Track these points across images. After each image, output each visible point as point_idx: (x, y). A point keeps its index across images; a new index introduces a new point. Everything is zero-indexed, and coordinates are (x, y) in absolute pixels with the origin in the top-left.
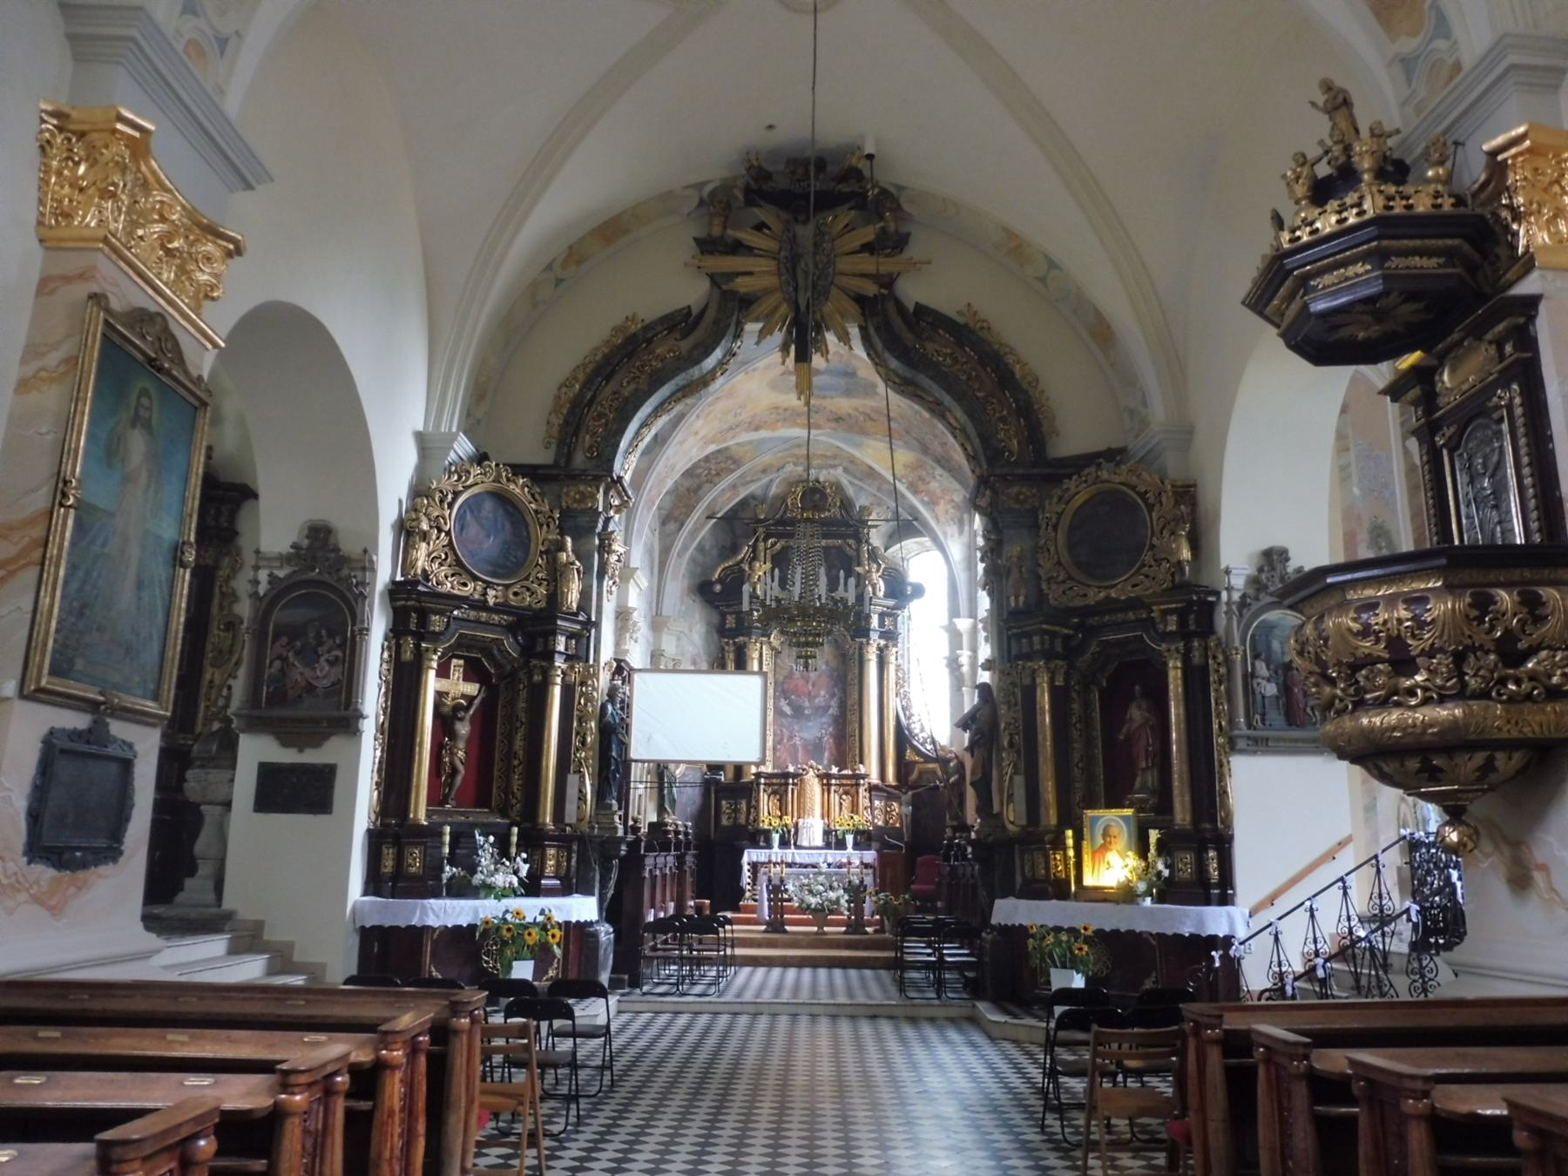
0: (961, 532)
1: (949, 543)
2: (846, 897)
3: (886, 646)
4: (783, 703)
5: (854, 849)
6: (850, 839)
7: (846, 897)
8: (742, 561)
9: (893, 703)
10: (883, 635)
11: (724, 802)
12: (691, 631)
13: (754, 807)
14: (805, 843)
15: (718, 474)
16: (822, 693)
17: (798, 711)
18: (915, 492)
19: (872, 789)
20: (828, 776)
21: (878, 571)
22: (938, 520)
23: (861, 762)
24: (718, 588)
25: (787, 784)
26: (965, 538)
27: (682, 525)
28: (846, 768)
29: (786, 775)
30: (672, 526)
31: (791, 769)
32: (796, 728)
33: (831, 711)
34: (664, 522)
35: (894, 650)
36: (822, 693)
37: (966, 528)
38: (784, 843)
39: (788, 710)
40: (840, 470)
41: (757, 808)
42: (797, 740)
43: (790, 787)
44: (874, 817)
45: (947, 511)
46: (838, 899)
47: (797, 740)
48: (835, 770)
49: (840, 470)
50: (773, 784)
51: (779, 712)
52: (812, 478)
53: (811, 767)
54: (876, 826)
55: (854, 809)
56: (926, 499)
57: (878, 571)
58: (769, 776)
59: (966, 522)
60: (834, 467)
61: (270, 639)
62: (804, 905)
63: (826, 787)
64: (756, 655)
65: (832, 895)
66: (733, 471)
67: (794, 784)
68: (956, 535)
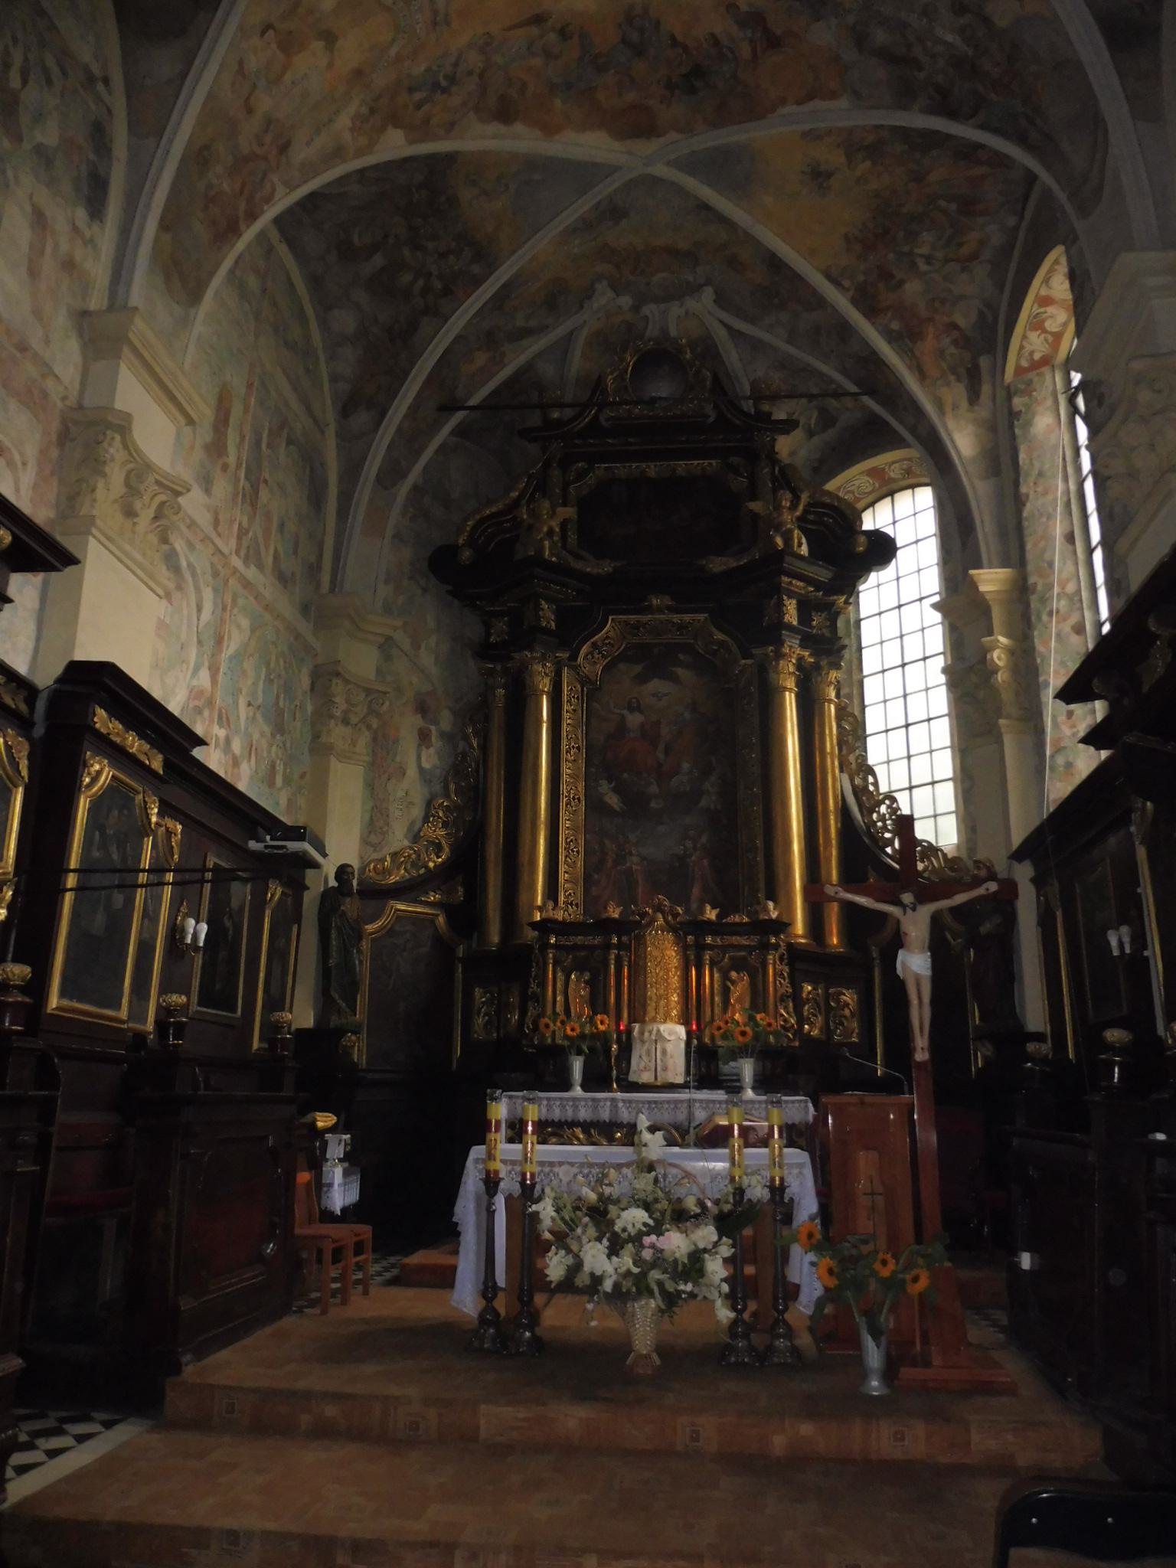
0: (974, 397)
1: (951, 424)
2: (725, 1251)
3: (817, 667)
4: (604, 787)
5: (585, 1087)
6: (747, 1069)
7: (725, 1251)
8: (516, 504)
9: (837, 783)
10: (807, 641)
11: (478, 992)
12: (416, 646)
13: (532, 999)
14: (646, 1078)
15: (447, 291)
16: (686, 766)
17: (636, 805)
18: (871, 312)
19: (794, 955)
20: (702, 927)
21: (793, 507)
22: (922, 375)
23: (772, 896)
24: (466, 555)
25: (608, 946)
26: (984, 411)
27: (383, 414)
28: (736, 910)
29: (605, 926)
30: (362, 418)
31: (614, 912)
32: (632, 838)
33: (703, 803)
34: (347, 408)
35: (834, 675)
36: (686, 766)
37: (986, 389)
38: (596, 1080)
39: (613, 800)
40: (705, 302)
41: (540, 999)
42: (634, 863)
43: (613, 954)
44: (801, 1021)
45: (942, 353)
46: (697, 1257)
47: (634, 863)
48: (711, 914)
49: (705, 302)
50: (576, 947)
51: (595, 806)
52: (652, 331)
53: (659, 908)
54: (807, 1039)
55: (757, 1000)
56: (895, 326)
57: (793, 507)
58: (564, 928)
59: (985, 376)
60: (694, 289)
61: (247, 909)
62: (582, 1280)
63: (692, 957)
64: (545, 684)
65: (676, 1243)
66: (477, 282)
67: (620, 946)
68: (964, 404)
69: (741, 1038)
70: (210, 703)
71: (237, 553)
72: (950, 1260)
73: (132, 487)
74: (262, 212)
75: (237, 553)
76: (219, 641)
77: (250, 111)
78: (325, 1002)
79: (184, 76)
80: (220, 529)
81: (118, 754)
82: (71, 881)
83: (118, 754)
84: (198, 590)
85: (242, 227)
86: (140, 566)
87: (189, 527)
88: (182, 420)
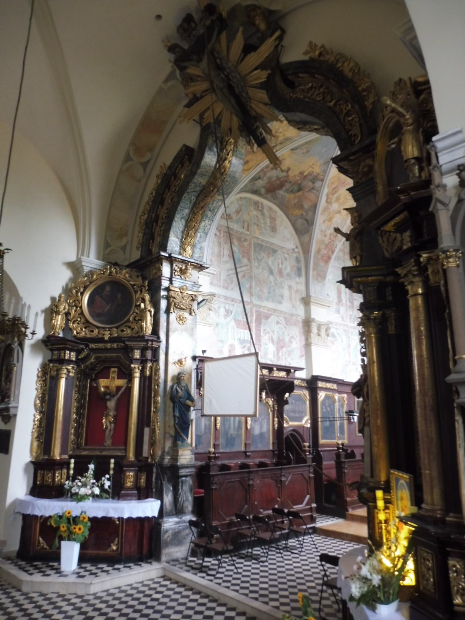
69: (349, 478)
70: (350, 362)
71: (350, 322)
72: (346, 501)
73: (319, 329)
74: (335, 250)
75: (350, 322)
76: (349, 346)
77: (325, 236)
78: (243, 506)
79: (310, 239)
80: (344, 320)
81: (326, 389)
82: (320, 420)
83: (326, 389)
84: (242, 529)
85: (331, 256)
86: (324, 346)
87: (336, 325)
88: (327, 307)
